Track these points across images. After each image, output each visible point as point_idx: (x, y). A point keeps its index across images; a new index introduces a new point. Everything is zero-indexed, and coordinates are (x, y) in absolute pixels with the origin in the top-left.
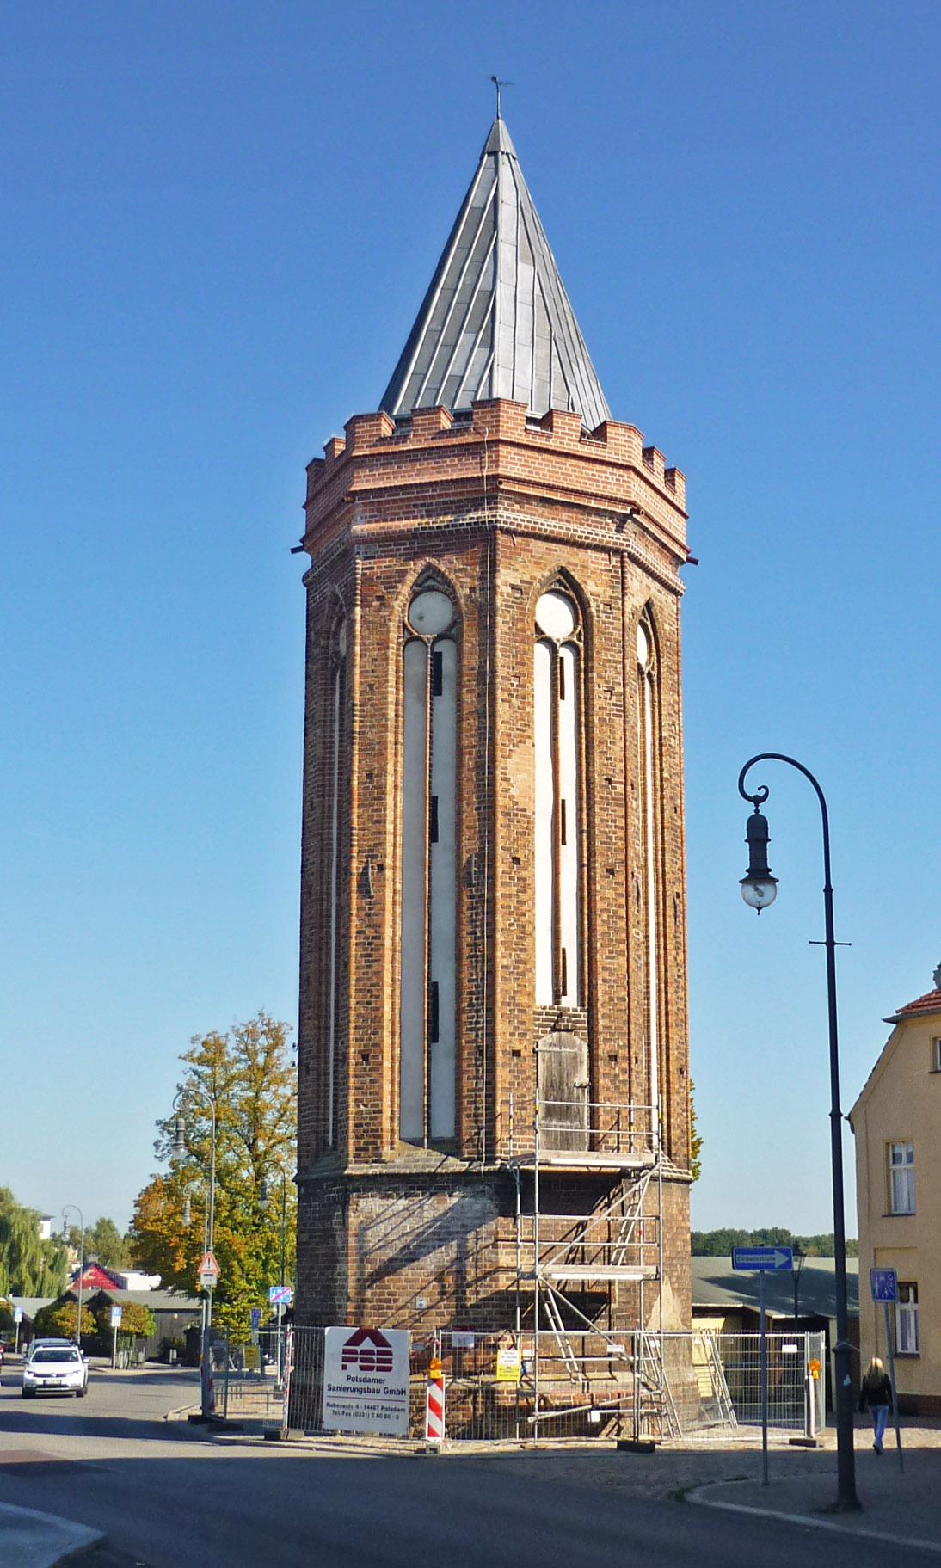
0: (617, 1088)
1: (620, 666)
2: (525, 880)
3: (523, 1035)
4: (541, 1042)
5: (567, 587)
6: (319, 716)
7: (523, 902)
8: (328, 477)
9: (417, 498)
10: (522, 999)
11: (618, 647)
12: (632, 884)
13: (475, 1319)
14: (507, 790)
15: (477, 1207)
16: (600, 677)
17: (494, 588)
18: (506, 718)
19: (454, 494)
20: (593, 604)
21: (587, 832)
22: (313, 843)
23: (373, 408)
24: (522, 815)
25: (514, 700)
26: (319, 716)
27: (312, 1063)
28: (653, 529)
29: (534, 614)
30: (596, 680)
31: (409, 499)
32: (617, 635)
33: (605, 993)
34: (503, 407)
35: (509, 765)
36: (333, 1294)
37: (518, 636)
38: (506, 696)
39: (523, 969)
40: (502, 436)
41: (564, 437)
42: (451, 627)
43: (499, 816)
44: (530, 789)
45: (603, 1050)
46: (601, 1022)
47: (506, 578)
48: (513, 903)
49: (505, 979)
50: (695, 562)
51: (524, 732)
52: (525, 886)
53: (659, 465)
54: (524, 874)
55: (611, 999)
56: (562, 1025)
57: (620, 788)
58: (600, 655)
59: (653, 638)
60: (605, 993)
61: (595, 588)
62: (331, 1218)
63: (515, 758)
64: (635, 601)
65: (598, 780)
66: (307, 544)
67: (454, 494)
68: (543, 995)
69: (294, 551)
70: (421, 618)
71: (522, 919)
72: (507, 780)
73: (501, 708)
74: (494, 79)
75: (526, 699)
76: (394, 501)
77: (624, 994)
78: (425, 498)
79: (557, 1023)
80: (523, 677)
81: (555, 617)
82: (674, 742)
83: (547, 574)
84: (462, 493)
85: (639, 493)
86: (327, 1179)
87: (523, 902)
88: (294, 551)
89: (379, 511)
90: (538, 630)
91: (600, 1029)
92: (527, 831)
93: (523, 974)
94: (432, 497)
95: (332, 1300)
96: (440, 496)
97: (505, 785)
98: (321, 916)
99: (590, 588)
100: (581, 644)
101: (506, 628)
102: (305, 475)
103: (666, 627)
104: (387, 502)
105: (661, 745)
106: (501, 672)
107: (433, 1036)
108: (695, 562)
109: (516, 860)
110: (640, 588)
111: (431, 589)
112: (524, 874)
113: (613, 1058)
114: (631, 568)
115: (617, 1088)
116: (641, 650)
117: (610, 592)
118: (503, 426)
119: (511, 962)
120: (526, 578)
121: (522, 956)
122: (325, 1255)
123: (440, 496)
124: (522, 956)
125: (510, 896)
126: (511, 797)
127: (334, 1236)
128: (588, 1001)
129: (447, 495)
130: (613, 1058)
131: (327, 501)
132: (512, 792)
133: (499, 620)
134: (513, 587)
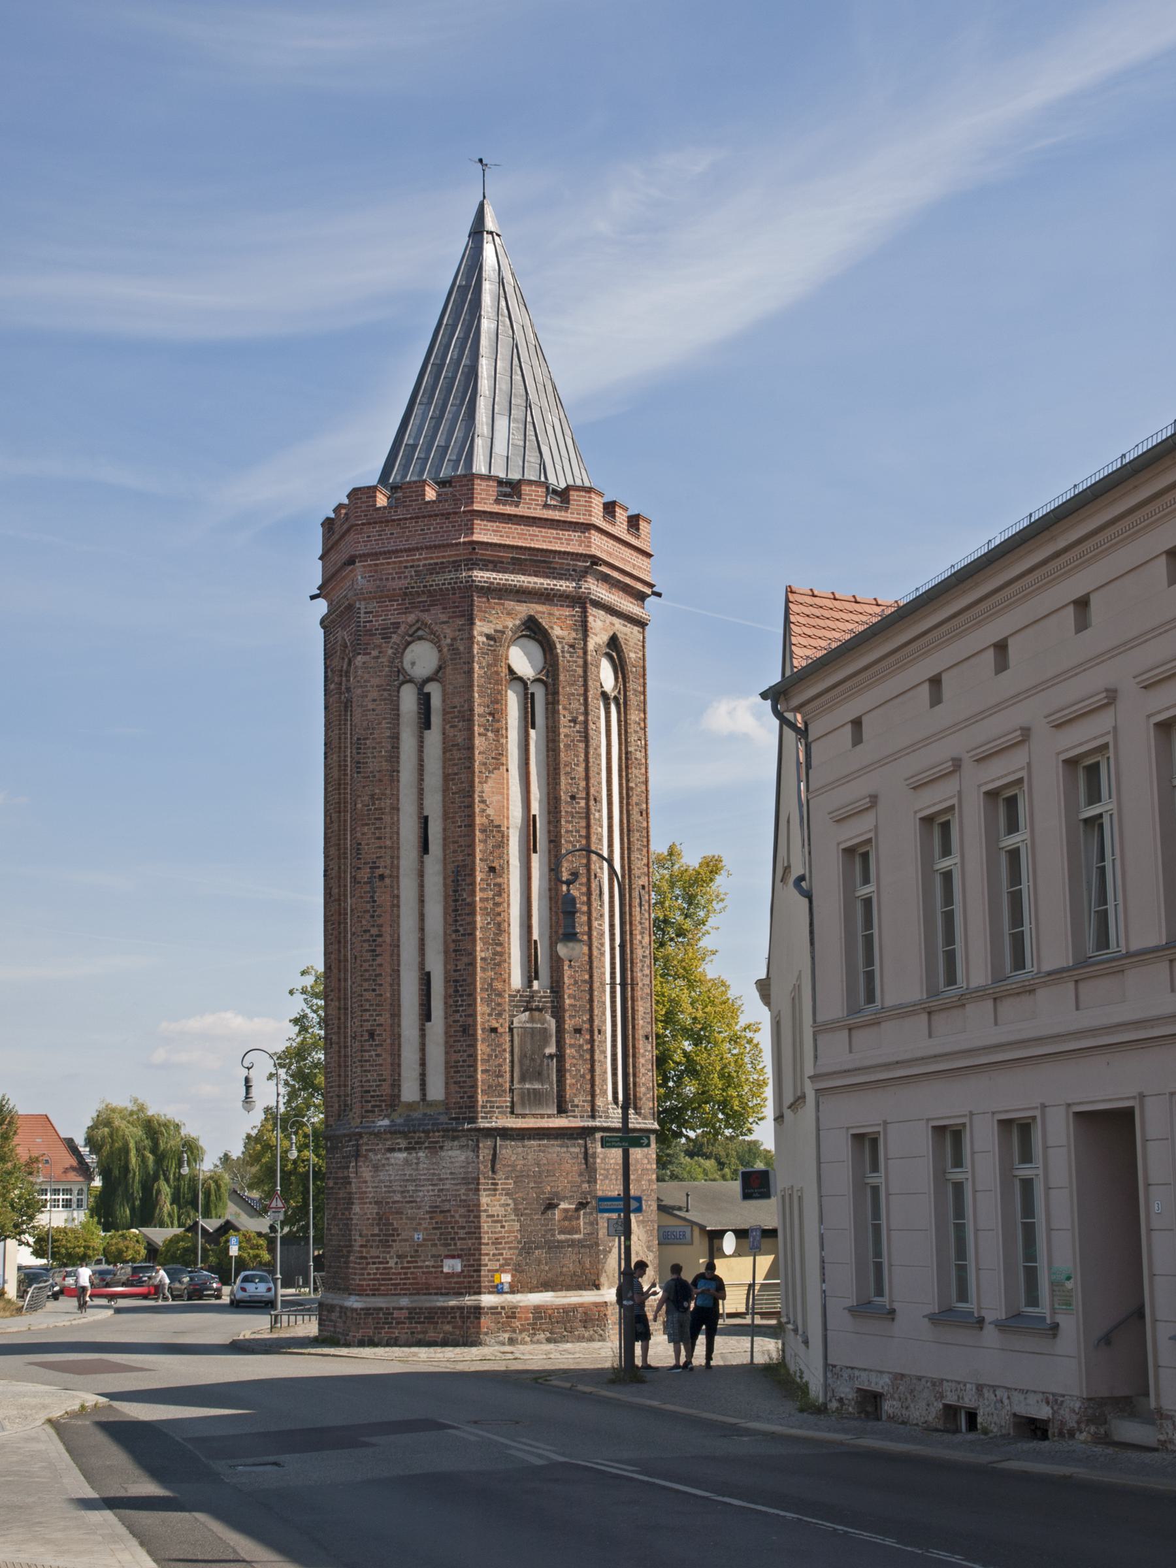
0: (581, 1056)
1: (582, 699)
2: (499, 885)
3: (500, 1015)
4: (515, 1020)
5: (533, 630)
6: (335, 743)
7: (497, 904)
8: (336, 537)
9: (407, 561)
10: (498, 985)
11: (581, 682)
12: (594, 885)
13: (462, 1250)
14: (484, 811)
15: (463, 1158)
16: (565, 708)
17: (471, 638)
18: (482, 749)
19: (438, 558)
20: (558, 646)
21: (554, 841)
22: (333, 851)
23: (373, 481)
24: (497, 832)
25: (490, 734)
26: (335, 743)
27: (334, 1038)
28: (615, 574)
29: (507, 659)
30: (562, 711)
31: (401, 562)
32: (580, 671)
33: (570, 977)
34: (477, 481)
35: (485, 789)
36: (350, 1230)
37: (492, 677)
38: (482, 730)
39: (499, 960)
40: (476, 507)
41: (532, 505)
42: (437, 672)
43: (477, 833)
44: (503, 809)
45: (569, 1024)
46: (567, 1001)
47: (481, 628)
48: (490, 905)
49: (484, 970)
50: (659, 595)
51: (498, 760)
52: (501, 890)
53: (621, 516)
54: (499, 880)
55: (576, 982)
56: (534, 1005)
57: (583, 803)
58: (565, 690)
59: (620, 667)
60: (570, 977)
61: (560, 632)
62: (348, 1167)
63: (490, 783)
64: (598, 638)
65: (564, 797)
66: (324, 591)
67: (438, 558)
68: (516, 980)
69: (313, 597)
70: (413, 664)
71: (498, 919)
72: (483, 802)
73: (478, 741)
74: (481, 161)
75: (499, 732)
76: (388, 563)
77: (587, 977)
78: (413, 560)
79: (528, 1004)
80: (496, 713)
81: (522, 660)
82: (639, 755)
83: (518, 622)
84: (443, 557)
85: (599, 546)
86: (345, 1135)
87: (497, 904)
88: (313, 597)
89: (376, 571)
90: (511, 671)
91: (567, 1007)
92: (502, 844)
93: (499, 964)
94: (419, 560)
95: (350, 1235)
96: (426, 559)
97: (482, 806)
98: (340, 914)
99: (557, 632)
100: (550, 680)
101: (482, 672)
102: (320, 530)
103: (632, 655)
104: (382, 564)
105: (627, 759)
106: (478, 710)
107: (788, 822)
108: (659, 595)
109: (492, 869)
110: (601, 627)
111: (420, 638)
112: (499, 880)
113: (578, 1031)
114: (592, 611)
115: (581, 1056)
116: (606, 676)
117: (574, 634)
118: (477, 497)
119: (488, 954)
120: (499, 627)
121: (498, 949)
122: (344, 1199)
123: (426, 559)
124: (498, 949)
125: (487, 899)
126: (488, 816)
127: (350, 1183)
128: (556, 988)
129: (432, 558)
130: (578, 1031)
131: (339, 557)
132: (489, 811)
133: (476, 666)
134: (489, 637)
